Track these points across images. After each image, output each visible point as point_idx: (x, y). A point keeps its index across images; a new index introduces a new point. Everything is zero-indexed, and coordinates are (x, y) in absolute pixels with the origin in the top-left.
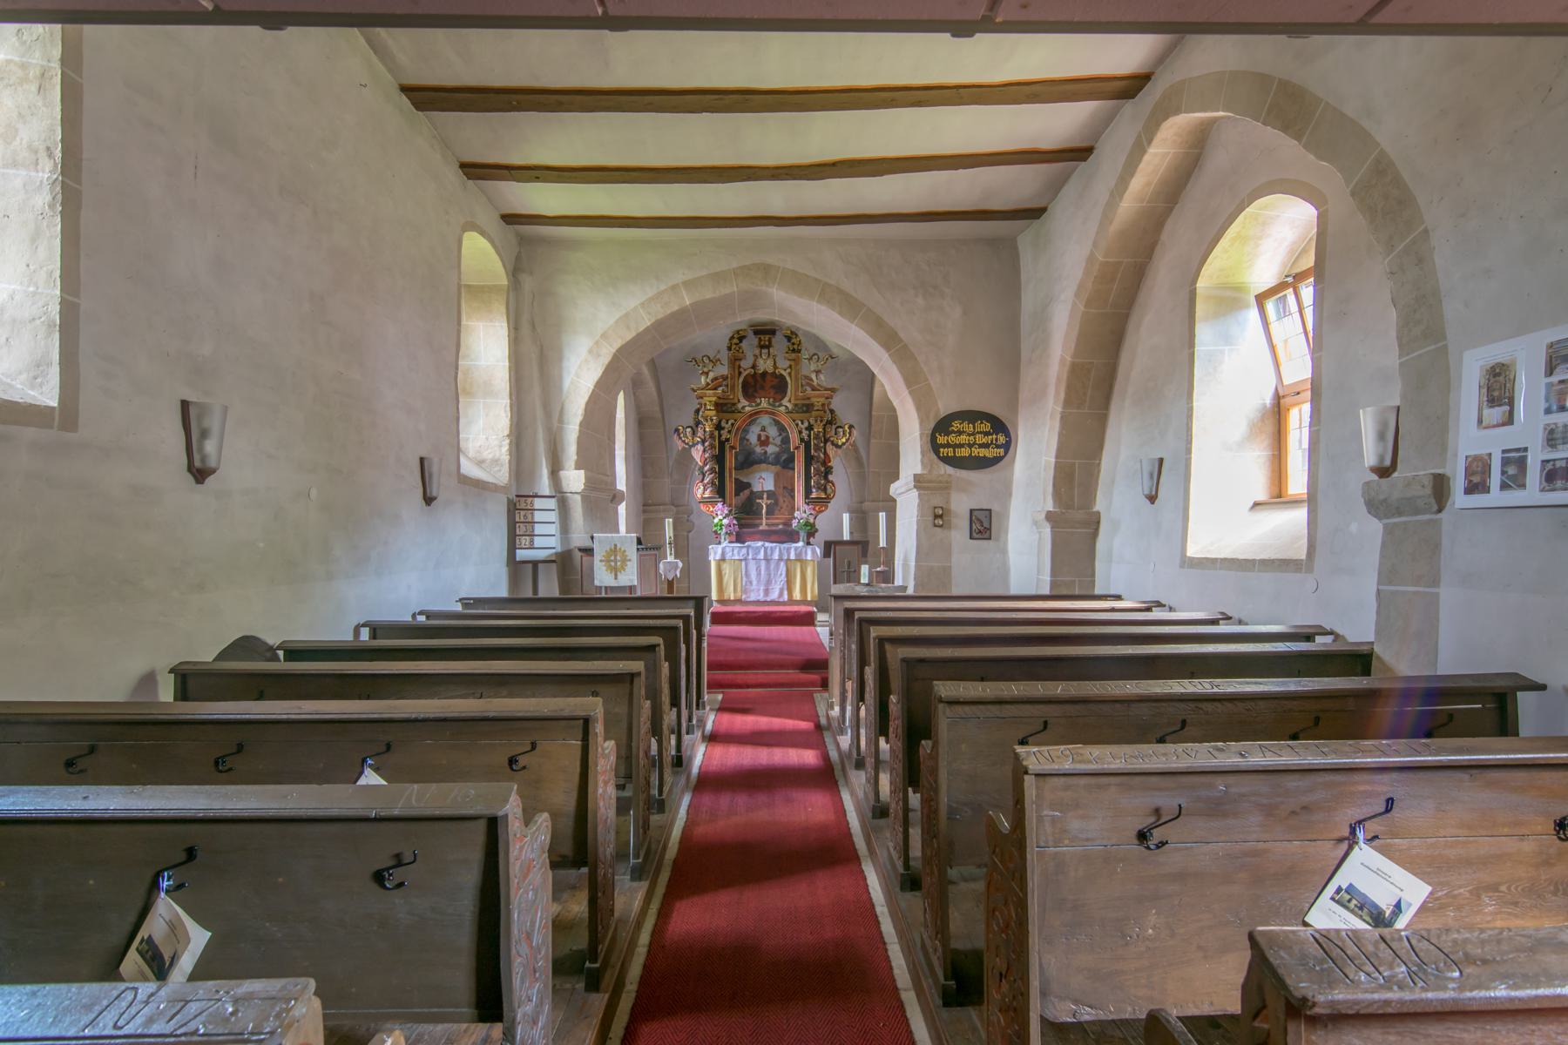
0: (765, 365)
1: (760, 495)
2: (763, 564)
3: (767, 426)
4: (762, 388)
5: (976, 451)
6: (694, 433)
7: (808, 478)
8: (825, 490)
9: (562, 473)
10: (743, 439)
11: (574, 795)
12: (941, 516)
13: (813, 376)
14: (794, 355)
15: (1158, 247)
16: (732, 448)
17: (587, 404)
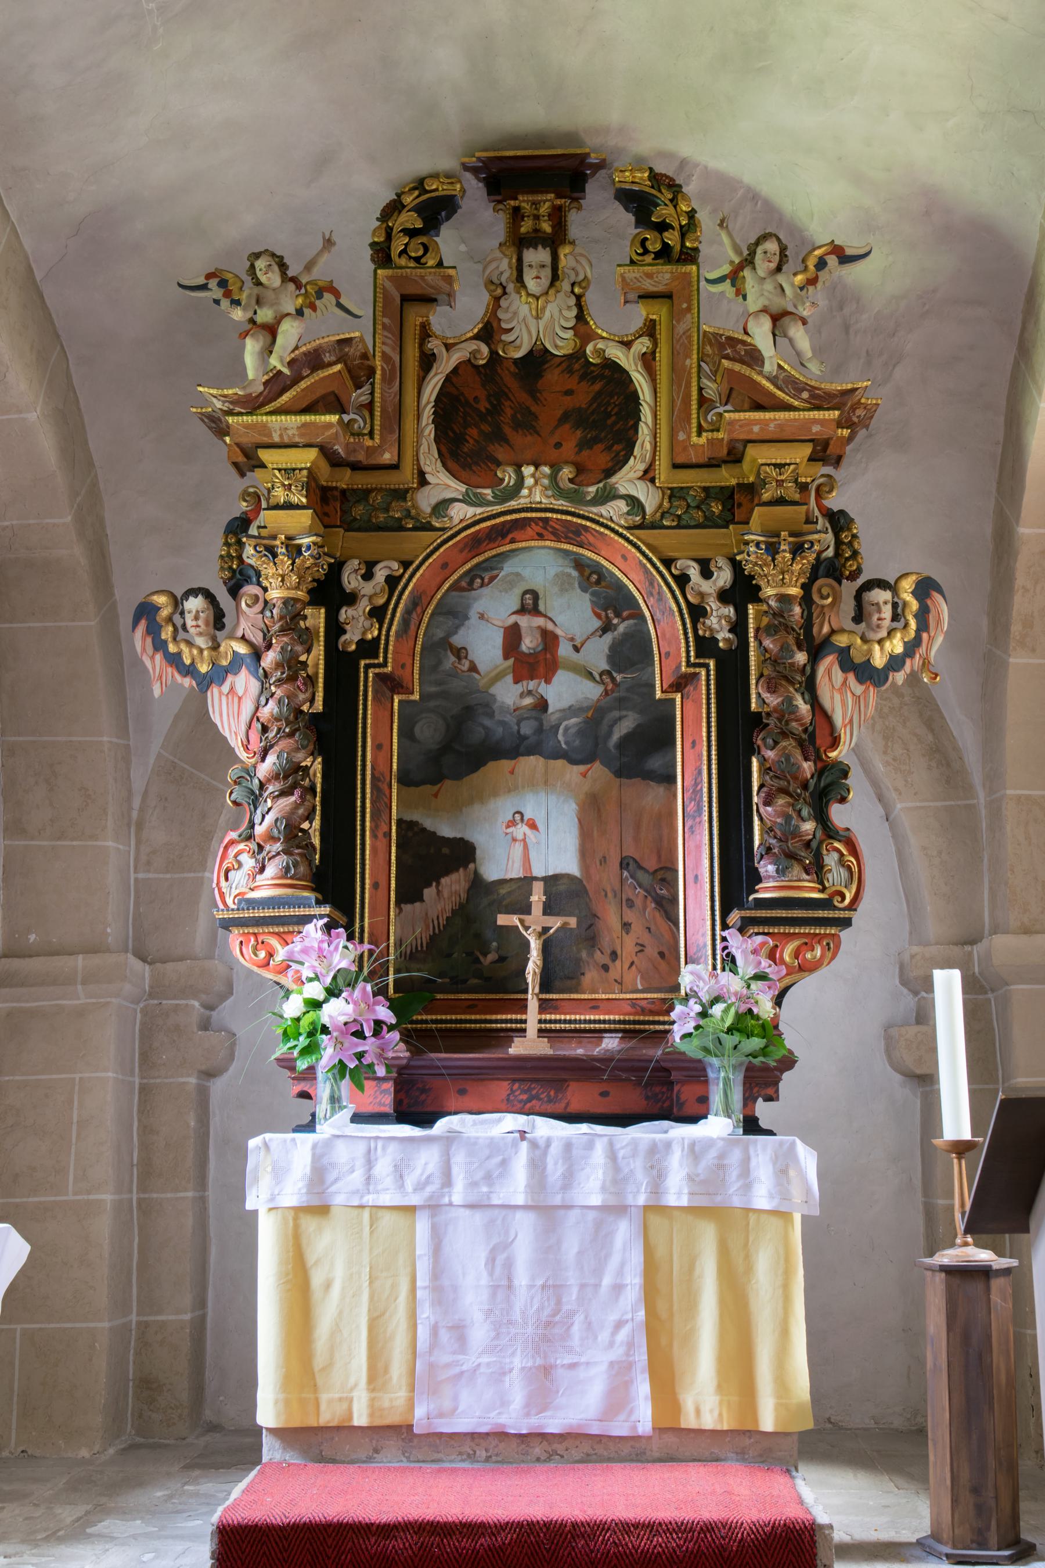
0: (538, 323)
1: (515, 895)
2: (524, 1230)
3: (545, 597)
4: (526, 422)
8: (817, 869)
10: (443, 648)
13: (761, 335)
14: (664, 275)
16: (391, 684)
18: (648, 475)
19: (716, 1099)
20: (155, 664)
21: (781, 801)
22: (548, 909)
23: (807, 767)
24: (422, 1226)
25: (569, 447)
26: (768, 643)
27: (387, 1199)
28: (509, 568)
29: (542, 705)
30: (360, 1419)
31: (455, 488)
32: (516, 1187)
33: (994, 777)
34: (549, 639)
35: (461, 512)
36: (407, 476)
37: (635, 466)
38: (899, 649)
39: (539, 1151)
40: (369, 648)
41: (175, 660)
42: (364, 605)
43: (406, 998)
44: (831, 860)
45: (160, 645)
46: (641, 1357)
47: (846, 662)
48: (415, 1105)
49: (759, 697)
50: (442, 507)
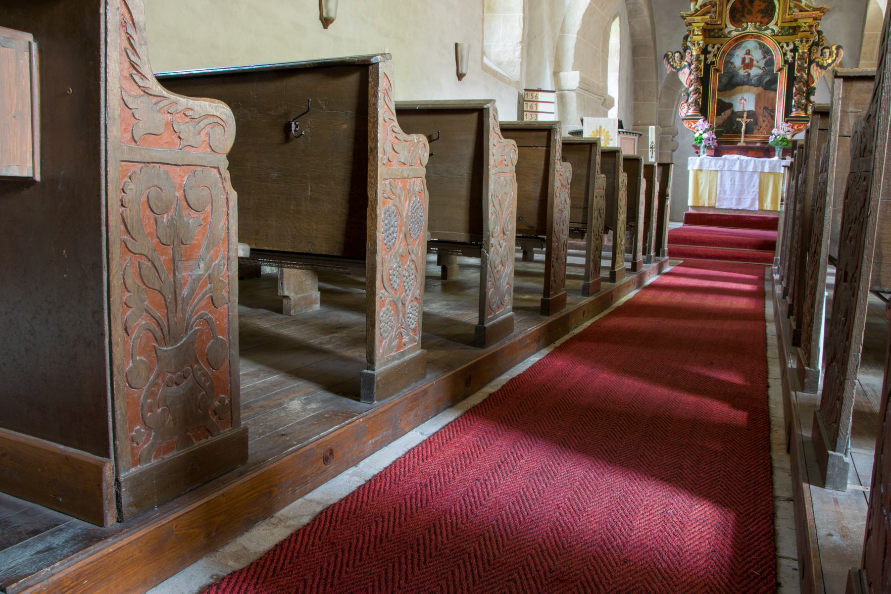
2: (738, 175)
4: (750, 13)
6: (682, 58)
7: (789, 97)
9: (563, 74)
10: (728, 63)
11: (540, 184)
16: (717, 70)
17: (584, 16)
18: (776, 24)
19: (777, 153)
20: (668, 67)
22: (747, 117)
23: (805, 89)
24: (719, 174)
25: (759, 18)
27: (713, 169)
28: (744, 45)
29: (749, 75)
30: (706, 205)
31: (733, 28)
32: (737, 167)
34: (752, 60)
35: (734, 33)
36: (723, 25)
37: (773, 22)
39: (741, 161)
40: (713, 63)
41: (672, 66)
42: (712, 54)
43: (717, 133)
45: (669, 63)
46: (757, 197)
47: (818, 65)
48: (718, 153)
49: (796, 74)
50: (730, 32)
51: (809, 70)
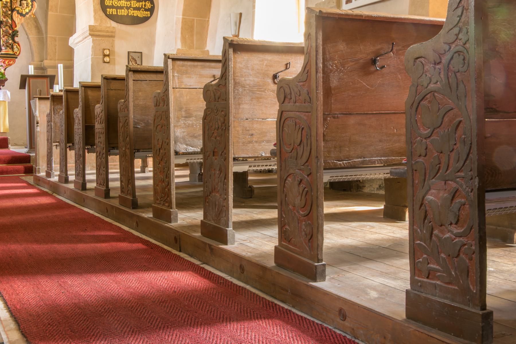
5: (131, 12)
8: (12, 48)
12: (108, 56)
15: (17, 328)
21: (6, 37)
23: (11, 31)
26: (4, 9)
33: (46, 32)
38: (28, 11)
44: (15, 47)
47: (18, 12)
51: (12, 16)
